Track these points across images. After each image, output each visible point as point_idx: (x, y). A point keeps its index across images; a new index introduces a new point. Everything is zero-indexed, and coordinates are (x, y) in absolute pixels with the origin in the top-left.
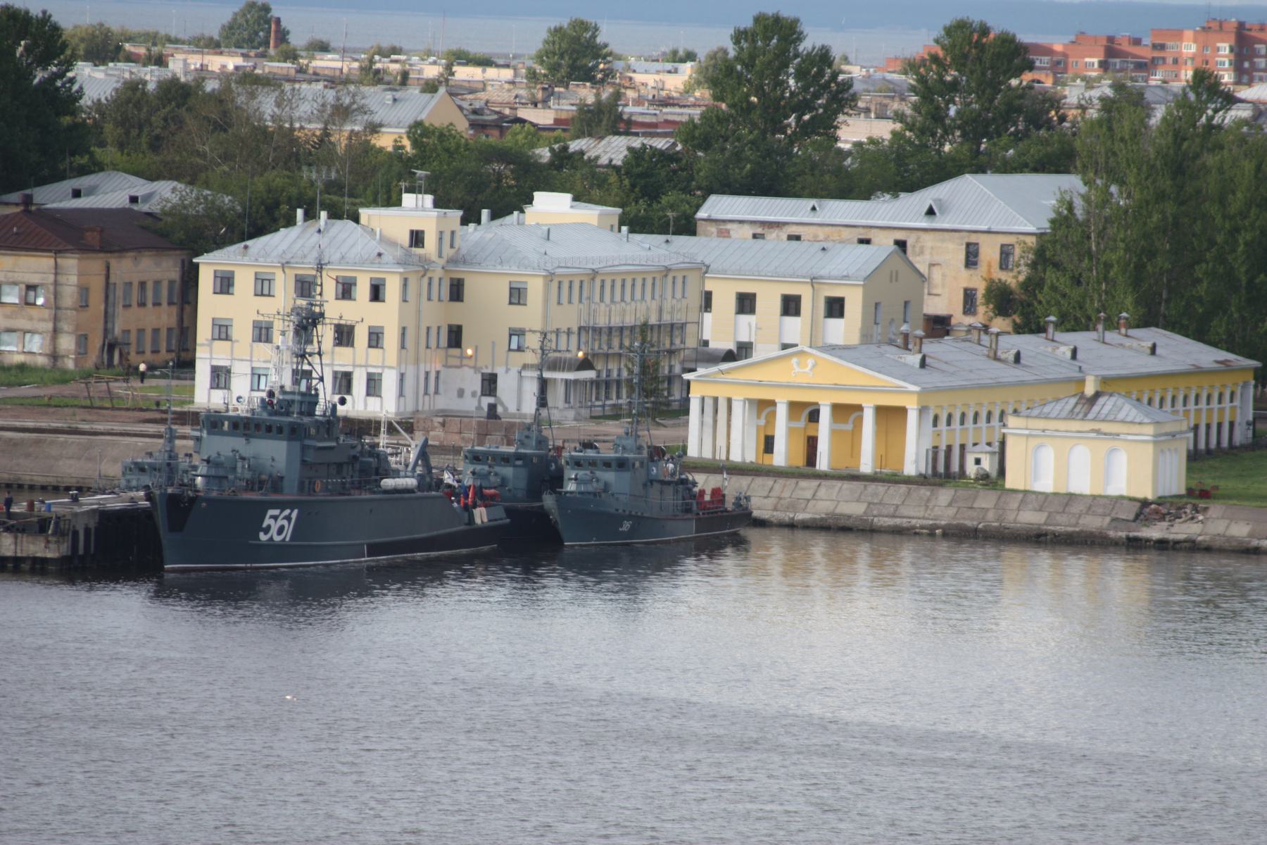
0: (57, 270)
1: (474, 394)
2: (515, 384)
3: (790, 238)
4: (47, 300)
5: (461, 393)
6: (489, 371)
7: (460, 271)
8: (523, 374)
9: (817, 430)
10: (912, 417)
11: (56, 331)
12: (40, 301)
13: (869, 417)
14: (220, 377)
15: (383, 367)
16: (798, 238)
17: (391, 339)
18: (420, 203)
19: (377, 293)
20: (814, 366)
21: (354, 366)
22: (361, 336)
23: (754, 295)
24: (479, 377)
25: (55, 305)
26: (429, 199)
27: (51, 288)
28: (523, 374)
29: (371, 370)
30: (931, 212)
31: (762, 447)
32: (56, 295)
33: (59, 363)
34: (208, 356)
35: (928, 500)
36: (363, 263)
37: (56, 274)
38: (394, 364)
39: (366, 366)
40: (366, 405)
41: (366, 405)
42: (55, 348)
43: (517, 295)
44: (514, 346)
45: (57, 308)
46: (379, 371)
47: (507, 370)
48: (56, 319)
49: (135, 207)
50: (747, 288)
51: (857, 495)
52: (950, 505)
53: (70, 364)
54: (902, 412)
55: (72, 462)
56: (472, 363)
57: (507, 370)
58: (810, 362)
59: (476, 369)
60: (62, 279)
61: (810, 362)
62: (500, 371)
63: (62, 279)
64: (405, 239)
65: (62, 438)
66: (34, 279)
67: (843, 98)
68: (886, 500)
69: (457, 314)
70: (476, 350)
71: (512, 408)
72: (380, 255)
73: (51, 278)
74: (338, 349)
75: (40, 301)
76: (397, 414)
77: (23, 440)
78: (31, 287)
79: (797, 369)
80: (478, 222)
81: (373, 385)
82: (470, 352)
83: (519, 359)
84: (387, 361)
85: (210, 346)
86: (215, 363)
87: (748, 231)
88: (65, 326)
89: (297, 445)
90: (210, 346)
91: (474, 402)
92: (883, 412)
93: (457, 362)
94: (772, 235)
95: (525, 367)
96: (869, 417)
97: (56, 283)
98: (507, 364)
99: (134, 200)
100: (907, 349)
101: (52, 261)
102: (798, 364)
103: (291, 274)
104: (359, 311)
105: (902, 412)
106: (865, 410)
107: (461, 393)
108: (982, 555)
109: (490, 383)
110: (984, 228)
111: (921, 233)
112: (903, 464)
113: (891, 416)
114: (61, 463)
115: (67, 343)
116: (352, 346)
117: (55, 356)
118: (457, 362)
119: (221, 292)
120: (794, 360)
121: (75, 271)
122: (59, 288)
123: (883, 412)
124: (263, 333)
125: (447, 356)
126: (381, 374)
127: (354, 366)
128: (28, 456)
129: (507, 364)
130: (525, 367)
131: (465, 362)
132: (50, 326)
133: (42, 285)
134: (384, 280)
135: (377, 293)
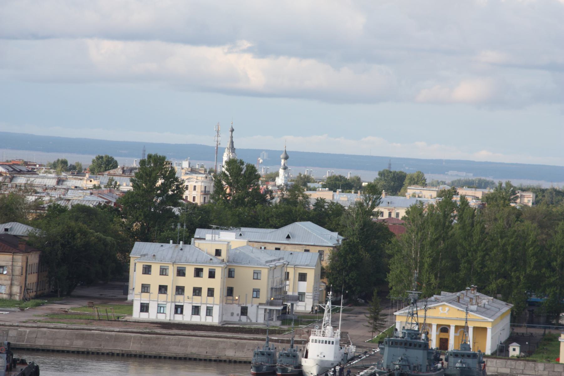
1: (238, 315)
2: (255, 311)
3: (277, 249)
4: (8, 272)
5: (232, 314)
6: (244, 306)
7: (233, 266)
8: (260, 307)
9: (449, 336)
10: (489, 332)
11: (12, 285)
12: (5, 272)
14: (144, 308)
15: (214, 304)
16: (279, 249)
17: (217, 293)
18: (213, 238)
19: (212, 275)
20: (448, 310)
21: (201, 304)
22: (205, 292)
23: (306, 274)
24: (240, 308)
25: (12, 275)
27: (10, 267)
28: (260, 307)
29: (208, 305)
30: (288, 237)
32: (12, 270)
33: (12, 298)
34: (139, 299)
35: (535, 368)
36: (206, 263)
37: (13, 262)
38: (218, 303)
39: (206, 304)
40: (206, 319)
41: (206, 319)
42: (11, 291)
43: (257, 275)
44: (255, 296)
45: (13, 275)
46: (211, 306)
47: (252, 305)
48: (12, 280)
49: (7, 232)
51: (504, 365)
52: (544, 370)
53: (17, 298)
54: (485, 329)
55: (175, 347)
56: (237, 302)
57: (252, 305)
58: (447, 309)
59: (239, 304)
60: (15, 264)
61: (447, 309)
62: (249, 306)
63: (15, 264)
64: (214, 253)
65: (167, 337)
68: (517, 367)
69: (231, 283)
70: (239, 297)
71: (254, 321)
72: (211, 259)
73: (10, 263)
74: (195, 297)
75: (5, 272)
76: (219, 323)
77: (151, 337)
79: (441, 312)
80: (169, 243)
81: (209, 312)
82: (237, 298)
83: (257, 301)
84: (216, 302)
85: (140, 295)
86: (142, 302)
88: (15, 282)
89: (426, 352)
90: (140, 295)
91: (238, 318)
93: (231, 302)
95: (260, 304)
97: (12, 265)
98: (252, 303)
99: (6, 230)
100: (459, 302)
101: (11, 256)
102: (442, 309)
103: (176, 266)
104: (204, 282)
105: (485, 329)
106: (451, 327)
107: (232, 314)
108: (232, 366)
109: (244, 311)
110: (313, 244)
111: (286, 246)
112: (485, 350)
113: (480, 331)
114: (171, 347)
115: (16, 289)
116: (201, 296)
117: (11, 294)
118: (231, 302)
119: (145, 274)
120: (440, 308)
121: (21, 261)
122: (14, 268)
125: (227, 299)
126: (148, 304)
127: (201, 304)
128: (156, 344)
129: (252, 303)
130: (260, 304)
131: (234, 302)
132: (9, 282)
133: (6, 266)
134: (185, 268)
135: (212, 275)
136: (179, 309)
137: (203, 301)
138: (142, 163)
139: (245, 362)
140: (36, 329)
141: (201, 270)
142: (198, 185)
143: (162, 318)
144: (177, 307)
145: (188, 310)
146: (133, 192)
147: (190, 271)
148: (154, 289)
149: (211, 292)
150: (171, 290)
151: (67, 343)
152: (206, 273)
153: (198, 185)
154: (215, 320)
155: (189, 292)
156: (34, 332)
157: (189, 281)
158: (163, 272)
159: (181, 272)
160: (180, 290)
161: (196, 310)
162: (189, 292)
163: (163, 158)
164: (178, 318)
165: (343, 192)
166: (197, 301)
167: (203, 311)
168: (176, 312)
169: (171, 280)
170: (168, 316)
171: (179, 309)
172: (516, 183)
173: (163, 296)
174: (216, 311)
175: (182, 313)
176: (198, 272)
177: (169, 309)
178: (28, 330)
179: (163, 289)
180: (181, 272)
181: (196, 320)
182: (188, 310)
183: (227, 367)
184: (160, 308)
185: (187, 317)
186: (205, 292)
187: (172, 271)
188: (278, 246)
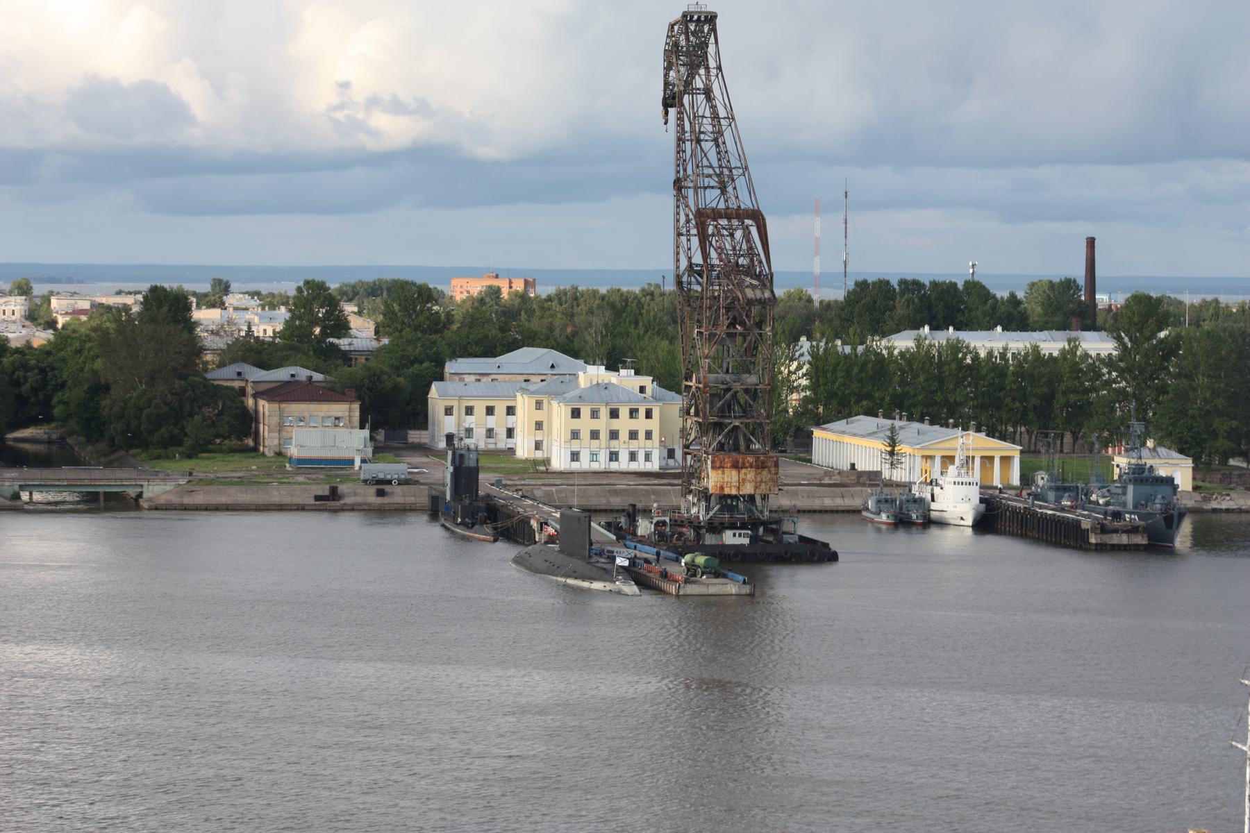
0: (350, 410)
13: (997, 462)
19: (649, 415)
22: (642, 435)
26: (603, 367)
30: (553, 366)
31: (253, 454)
50: (490, 404)
66: (339, 415)
67: (453, 322)
78: (337, 418)
81: (648, 457)
87: (473, 378)
92: (1003, 459)
94: (484, 379)
96: (997, 462)
99: (293, 376)
104: (641, 424)
108: (840, 515)
113: (1006, 460)
123: (1003, 459)
124: (490, 433)
135: (649, 415)
136: (614, 456)
137: (640, 445)
138: (299, 290)
139: (854, 511)
140: (816, 488)
141: (637, 410)
142: (17, 309)
143: (595, 466)
144: (612, 453)
145: (624, 456)
146: (130, 320)
147: (624, 412)
148: (585, 435)
149: (649, 435)
150: (604, 435)
151: (604, 501)
152: (642, 413)
153: (17, 309)
154: (654, 466)
155: (624, 436)
156: (561, 491)
157: (624, 424)
158: (595, 414)
159: (614, 414)
160: (633, 435)
161: (633, 456)
162: (624, 436)
163: (323, 283)
164: (614, 466)
165: (169, 307)
166: (634, 445)
167: (641, 457)
168: (611, 460)
169: (603, 423)
170: (602, 464)
171: (614, 456)
172: (187, 287)
173: (595, 442)
174: (656, 455)
175: (617, 460)
176: (633, 413)
177: (603, 456)
178: (554, 489)
179: (595, 435)
180: (614, 414)
181: (634, 466)
182: (624, 456)
183: (827, 517)
184: (594, 456)
185: (624, 464)
186: (642, 435)
187: (604, 412)
188: (526, 377)
